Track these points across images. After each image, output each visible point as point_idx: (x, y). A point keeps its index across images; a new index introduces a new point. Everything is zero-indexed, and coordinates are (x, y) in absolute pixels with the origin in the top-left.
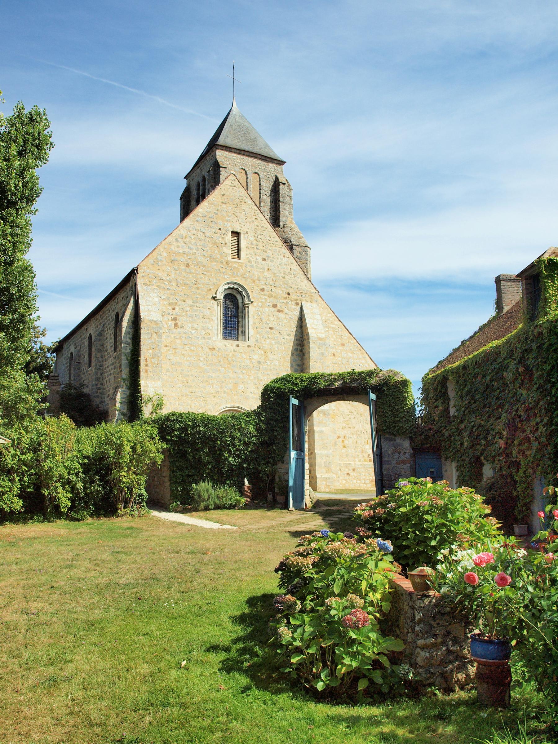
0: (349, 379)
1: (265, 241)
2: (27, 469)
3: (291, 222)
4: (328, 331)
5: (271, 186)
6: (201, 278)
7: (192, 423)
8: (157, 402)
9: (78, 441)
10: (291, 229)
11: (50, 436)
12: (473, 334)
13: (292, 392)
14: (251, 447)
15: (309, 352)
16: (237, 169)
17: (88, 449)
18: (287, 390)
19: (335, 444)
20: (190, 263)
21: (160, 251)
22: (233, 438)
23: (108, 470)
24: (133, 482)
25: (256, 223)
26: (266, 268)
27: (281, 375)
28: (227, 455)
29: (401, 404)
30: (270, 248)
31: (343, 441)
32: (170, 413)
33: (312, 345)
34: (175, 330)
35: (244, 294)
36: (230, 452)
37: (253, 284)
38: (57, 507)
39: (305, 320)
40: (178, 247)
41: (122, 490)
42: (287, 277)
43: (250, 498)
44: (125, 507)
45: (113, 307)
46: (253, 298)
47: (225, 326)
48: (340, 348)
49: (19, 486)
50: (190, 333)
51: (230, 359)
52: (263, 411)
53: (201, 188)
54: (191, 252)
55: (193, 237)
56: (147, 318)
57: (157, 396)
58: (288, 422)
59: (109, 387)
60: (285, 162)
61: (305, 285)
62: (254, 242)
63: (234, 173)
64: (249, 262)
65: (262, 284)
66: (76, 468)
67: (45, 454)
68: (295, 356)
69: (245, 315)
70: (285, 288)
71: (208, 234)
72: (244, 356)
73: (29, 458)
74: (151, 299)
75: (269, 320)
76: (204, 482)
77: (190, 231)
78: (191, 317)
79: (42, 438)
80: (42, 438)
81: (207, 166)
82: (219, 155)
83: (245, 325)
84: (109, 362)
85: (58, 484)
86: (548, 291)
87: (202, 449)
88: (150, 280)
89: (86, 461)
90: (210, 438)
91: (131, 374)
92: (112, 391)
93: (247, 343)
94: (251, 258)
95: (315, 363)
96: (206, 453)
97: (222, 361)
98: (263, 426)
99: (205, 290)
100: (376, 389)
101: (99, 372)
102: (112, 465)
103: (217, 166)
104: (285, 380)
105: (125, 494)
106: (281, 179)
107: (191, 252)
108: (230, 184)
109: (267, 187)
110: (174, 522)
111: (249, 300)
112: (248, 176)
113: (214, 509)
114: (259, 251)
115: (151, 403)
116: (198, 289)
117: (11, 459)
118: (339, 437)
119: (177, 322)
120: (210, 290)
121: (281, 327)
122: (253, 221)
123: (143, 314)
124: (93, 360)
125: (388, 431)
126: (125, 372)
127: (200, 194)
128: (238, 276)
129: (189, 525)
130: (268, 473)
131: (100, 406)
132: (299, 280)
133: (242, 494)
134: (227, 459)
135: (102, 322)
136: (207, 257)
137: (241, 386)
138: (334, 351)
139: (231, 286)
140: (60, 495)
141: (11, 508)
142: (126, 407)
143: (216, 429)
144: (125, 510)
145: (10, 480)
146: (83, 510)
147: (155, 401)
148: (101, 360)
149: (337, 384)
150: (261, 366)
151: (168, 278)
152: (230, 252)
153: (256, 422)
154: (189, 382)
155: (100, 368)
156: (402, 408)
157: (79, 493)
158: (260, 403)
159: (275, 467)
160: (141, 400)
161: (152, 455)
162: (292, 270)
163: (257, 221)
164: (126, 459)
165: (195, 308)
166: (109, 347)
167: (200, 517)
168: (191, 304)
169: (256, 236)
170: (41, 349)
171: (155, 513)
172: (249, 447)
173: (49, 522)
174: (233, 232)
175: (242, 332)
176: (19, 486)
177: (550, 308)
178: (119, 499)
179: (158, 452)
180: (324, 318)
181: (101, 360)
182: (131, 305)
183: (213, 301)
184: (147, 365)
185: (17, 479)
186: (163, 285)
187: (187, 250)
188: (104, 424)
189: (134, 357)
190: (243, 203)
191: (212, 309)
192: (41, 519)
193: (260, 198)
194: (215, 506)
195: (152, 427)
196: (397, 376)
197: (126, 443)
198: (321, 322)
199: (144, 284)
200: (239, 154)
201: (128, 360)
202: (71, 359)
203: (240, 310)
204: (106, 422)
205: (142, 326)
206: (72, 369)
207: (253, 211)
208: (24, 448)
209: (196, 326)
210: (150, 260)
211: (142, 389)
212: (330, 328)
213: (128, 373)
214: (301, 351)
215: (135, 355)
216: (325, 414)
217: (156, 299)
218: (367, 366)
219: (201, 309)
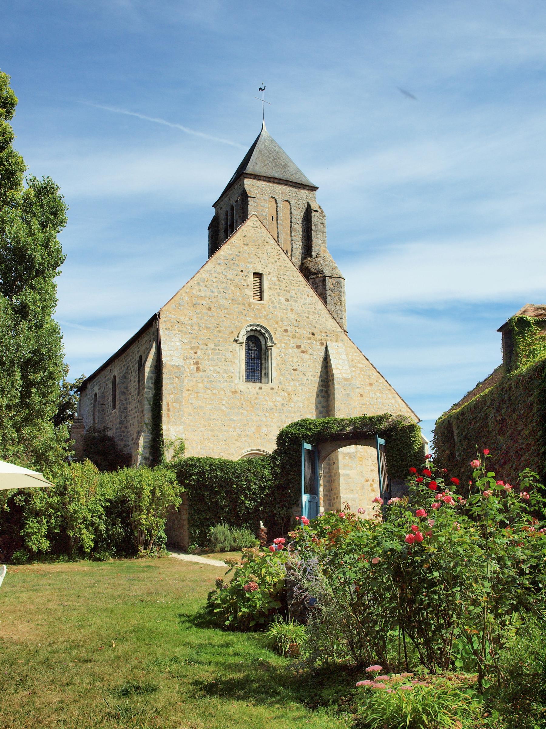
0: (360, 424)
1: (288, 282)
2: (54, 512)
3: (324, 252)
4: (354, 371)
5: (302, 214)
6: (223, 321)
7: (210, 467)
8: (178, 447)
9: (101, 485)
10: (324, 259)
11: (75, 481)
12: (488, 376)
13: (305, 437)
14: (267, 491)
15: (334, 394)
16: (267, 198)
17: (110, 494)
18: (301, 436)
19: (363, 487)
20: (212, 307)
21: (182, 295)
22: (249, 482)
23: (129, 513)
24: (152, 524)
25: (278, 264)
26: (289, 308)
27: (296, 420)
28: (244, 499)
29: (409, 448)
30: (293, 288)
31: (372, 485)
32: (189, 458)
33: (336, 386)
34: (197, 374)
35: (267, 335)
36: (246, 496)
37: (276, 326)
38: (82, 547)
39: (330, 360)
40: (200, 290)
41: (141, 533)
42: (311, 317)
43: (265, 541)
44: (145, 549)
45: (137, 350)
46: (277, 339)
47: (248, 369)
48: (367, 388)
49: (47, 527)
50: (212, 376)
51: (253, 402)
52: (278, 455)
53: (229, 217)
54: (213, 295)
55: (215, 280)
56: (169, 363)
57: (179, 441)
58: (301, 466)
59: (133, 430)
60: (317, 188)
61: (331, 324)
62: (277, 283)
63: (256, 214)
64: (272, 303)
65: (285, 325)
66: (99, 511)
67: (70, 498)
68: (320, 397)
69: (268, 357)
70: (309, 328)
71: (230, 277)
72: (267, 398)
73: (56, 501)
74: (173, 344)
75: (292, 361)
76: (221, 525)
77: (211, 274)
78: (213, 360)
79: (67, 483)
80: (67, 483)
81: (235, 197)
82: (247, 184)
83: (268, 367)
84: (133, 405)
85: (83, 526)
86: (519, 347)
87: (218, 493)
88: (172, 324)
89: (108, 504)
90: (226, 482)
91: (153, 419)
92: (135, 435)
93: (270, 385)
94: (273, 299)
95: (340, 405)
96: (223, 496)
97: (244, 403)
98: (278, 470)
99: (228, 332)
100: (384, 434)
101: (123, 415)
102: (132, 509)
103: (245, 196)
104: (300, 426)
105: (145, 536)
106: (314, 206)
107: (213, 295)
108: (252, 225)
109: (299, 214)
110: (190, 562)
111: (272, 341)
112: (278, 205)
113: (230, 551)
114: (282, 292)
115: (173, 448)
116: (220, 332)
117: (39, 502)
118: (367, 481)
119: (199, 365)
120: (232, 332)
121: (305, 368)
122: (276, 262)
123: (165, 360)
124: (117, 403)
125: (397, 475)
126: (148, 417)
127: (229, 224)
128: (260, 318)
129: (203, 564)
130: (283, 516)
131: (124, 449)
132: (324, 320)
133: (258, 536)
134: (243, 502)
135: (126, 364)
136: (229, 300)
137: (264, 429)
138: (361, 391)
139: (254, 328)
140: (84, 536)
141: (38, 548)
142: (148, 451)
143: (233, 473)
144: (145, 551)
145: (38, 522)
146: (105, 551)
147: (177, 446)
148: (125, 402)
149: (348, 429)
150: (285, 409)
151: (190, 322)
152: (252, 294)
153: (271, 466)
154: (212, 425)
155: (124, 410)
156: (410, 452)
157: (102, 535)
158: (276, 448)
159: (290, 510)
160: (163, 445)
161: (171, 499)
162: (317, 309)
163: (280, 261)
164: (146, 502)
165: (217, 351)
166: (132, 390)
167: (215, 558)
168: (213, 347)
169: (279, 276)
170: (64, 386)
171: (174, 555)
172: (265, 490)
173: (74, 561)
174: (255, 274)
175: (265, 374)
176: (47, 527)
177: (521, 363)
178: (140, 541)
179: (177, 496)
180: (350, 357)
181: (125, 402)
182: (153, 351)
183: (235, 343)
184: (168, 410)
185: (44, 521)
186: (185, 329)
187: (208, 294)
188: (125, 469)
189: (156, 402)
190: (265, 243)
191: (234, 351)
192: (66, 559)
193: (291, 227)
194: (231, 548)
195: (171, 472)
196: (406, 421)
197: (145, 487)
198: (346, 362)
199: (166, 329)
200: (269, 181)
201: (150, 405)
202: (95, 400)
203: (263, 352)
204: (128, 467)
205: (164, 371)
206: (96, 410)
207: (276, 251)
208: (51, 492)
209: (218, 369)
210: (172, 305)
211: (164, 434)
212: (358, 367)
213: (150, 418)
214: (327, 392)
215: (157, 400)
216: (350, 457)
217: (178, 344)
218: (397, 405)
219: (224, 352)
